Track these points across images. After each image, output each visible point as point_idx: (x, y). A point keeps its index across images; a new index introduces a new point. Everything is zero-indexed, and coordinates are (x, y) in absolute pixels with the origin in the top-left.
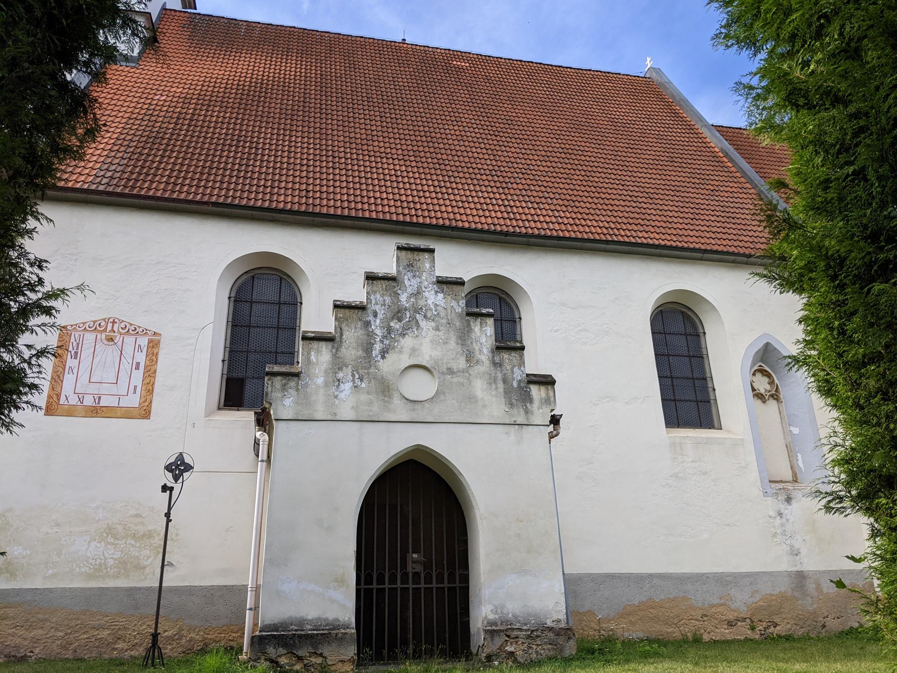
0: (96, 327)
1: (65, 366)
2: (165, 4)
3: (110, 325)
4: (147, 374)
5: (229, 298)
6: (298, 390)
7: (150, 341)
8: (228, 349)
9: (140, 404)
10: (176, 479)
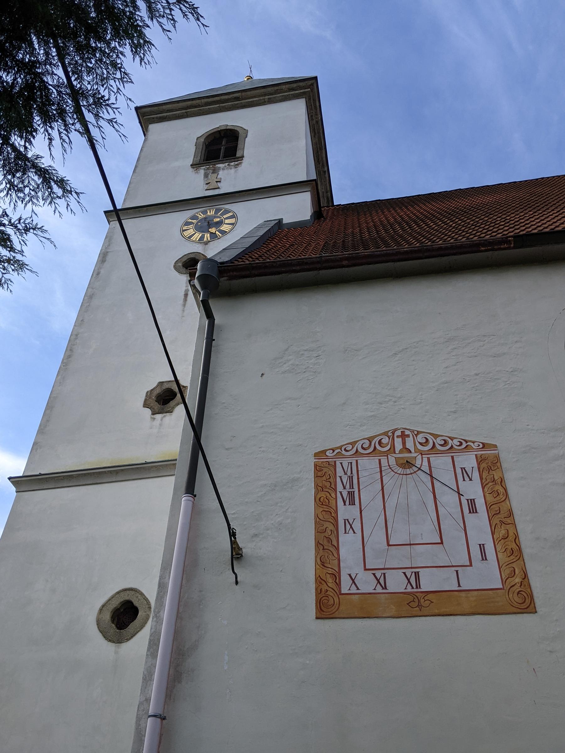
0: (374, 447)
1: (336, 519)
4: (496, 520)
7: (480, 460)
9: (504, 582)
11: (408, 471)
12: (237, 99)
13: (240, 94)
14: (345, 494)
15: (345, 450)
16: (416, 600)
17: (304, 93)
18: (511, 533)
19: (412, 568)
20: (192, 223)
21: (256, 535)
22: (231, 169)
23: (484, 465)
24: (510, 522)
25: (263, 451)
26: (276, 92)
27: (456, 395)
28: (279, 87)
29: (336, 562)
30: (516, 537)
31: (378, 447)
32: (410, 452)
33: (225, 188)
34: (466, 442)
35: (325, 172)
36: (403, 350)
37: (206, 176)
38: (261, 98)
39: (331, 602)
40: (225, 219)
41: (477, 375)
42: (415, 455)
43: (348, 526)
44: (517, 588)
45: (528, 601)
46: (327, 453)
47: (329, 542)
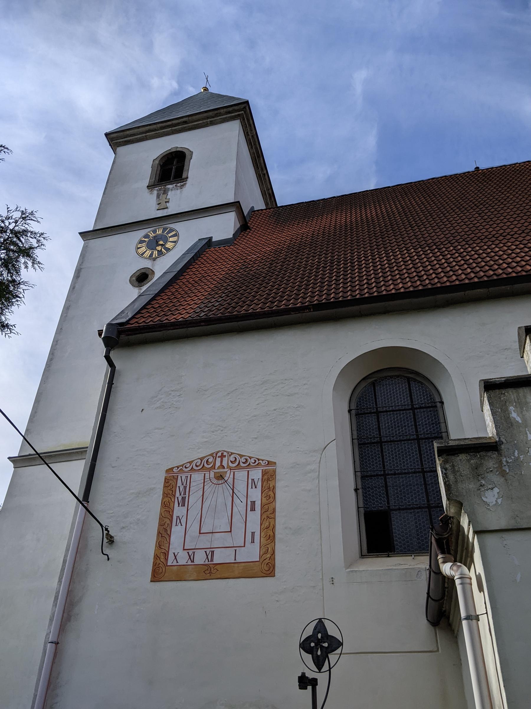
0: (202, 465)
1: (172, 516)
2: (253, 207)
3: (218, 460)
4: (265, 516)
5: (350, 411)
6: (503, 474)
7: (264, 473)
8: (359, 474)
9: (260, 557)
10: (319, 663)
11: (220, 482)
12: (185, 122)
13: (187, 118)
14: (180, 499)
15: (186, 468)
16: (209, 569)
17: (239, 115)
18: (271, 525)
19: (210, 548)
20: (145, 241)
21: (123, 528)
22: (177, 189)
23: (266, 477)
24: (272, 517)
25: (135, 469)
26: (216, 115)
27: (260, 425)
28: (219, 111)
29: (167, 545)
30: (274, 527)
31: (206, 465)
32: (224, 468)
33: (172, 209)
34: (259, 460)
35: (264, 174)
36: (234, 390)
37: (158, 196)
38: (205, 121)
39: (161, 571)
40: (170, 237)
41: (275, 410)
42: (226, 470)
43: (178, 521)
44: (267, 561)
45: (271, 569)
46: (174, 470)
47: (165, 531)
